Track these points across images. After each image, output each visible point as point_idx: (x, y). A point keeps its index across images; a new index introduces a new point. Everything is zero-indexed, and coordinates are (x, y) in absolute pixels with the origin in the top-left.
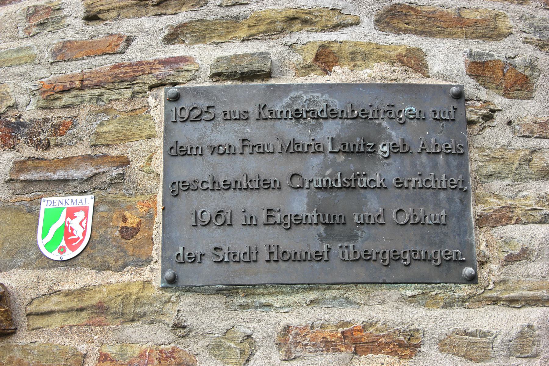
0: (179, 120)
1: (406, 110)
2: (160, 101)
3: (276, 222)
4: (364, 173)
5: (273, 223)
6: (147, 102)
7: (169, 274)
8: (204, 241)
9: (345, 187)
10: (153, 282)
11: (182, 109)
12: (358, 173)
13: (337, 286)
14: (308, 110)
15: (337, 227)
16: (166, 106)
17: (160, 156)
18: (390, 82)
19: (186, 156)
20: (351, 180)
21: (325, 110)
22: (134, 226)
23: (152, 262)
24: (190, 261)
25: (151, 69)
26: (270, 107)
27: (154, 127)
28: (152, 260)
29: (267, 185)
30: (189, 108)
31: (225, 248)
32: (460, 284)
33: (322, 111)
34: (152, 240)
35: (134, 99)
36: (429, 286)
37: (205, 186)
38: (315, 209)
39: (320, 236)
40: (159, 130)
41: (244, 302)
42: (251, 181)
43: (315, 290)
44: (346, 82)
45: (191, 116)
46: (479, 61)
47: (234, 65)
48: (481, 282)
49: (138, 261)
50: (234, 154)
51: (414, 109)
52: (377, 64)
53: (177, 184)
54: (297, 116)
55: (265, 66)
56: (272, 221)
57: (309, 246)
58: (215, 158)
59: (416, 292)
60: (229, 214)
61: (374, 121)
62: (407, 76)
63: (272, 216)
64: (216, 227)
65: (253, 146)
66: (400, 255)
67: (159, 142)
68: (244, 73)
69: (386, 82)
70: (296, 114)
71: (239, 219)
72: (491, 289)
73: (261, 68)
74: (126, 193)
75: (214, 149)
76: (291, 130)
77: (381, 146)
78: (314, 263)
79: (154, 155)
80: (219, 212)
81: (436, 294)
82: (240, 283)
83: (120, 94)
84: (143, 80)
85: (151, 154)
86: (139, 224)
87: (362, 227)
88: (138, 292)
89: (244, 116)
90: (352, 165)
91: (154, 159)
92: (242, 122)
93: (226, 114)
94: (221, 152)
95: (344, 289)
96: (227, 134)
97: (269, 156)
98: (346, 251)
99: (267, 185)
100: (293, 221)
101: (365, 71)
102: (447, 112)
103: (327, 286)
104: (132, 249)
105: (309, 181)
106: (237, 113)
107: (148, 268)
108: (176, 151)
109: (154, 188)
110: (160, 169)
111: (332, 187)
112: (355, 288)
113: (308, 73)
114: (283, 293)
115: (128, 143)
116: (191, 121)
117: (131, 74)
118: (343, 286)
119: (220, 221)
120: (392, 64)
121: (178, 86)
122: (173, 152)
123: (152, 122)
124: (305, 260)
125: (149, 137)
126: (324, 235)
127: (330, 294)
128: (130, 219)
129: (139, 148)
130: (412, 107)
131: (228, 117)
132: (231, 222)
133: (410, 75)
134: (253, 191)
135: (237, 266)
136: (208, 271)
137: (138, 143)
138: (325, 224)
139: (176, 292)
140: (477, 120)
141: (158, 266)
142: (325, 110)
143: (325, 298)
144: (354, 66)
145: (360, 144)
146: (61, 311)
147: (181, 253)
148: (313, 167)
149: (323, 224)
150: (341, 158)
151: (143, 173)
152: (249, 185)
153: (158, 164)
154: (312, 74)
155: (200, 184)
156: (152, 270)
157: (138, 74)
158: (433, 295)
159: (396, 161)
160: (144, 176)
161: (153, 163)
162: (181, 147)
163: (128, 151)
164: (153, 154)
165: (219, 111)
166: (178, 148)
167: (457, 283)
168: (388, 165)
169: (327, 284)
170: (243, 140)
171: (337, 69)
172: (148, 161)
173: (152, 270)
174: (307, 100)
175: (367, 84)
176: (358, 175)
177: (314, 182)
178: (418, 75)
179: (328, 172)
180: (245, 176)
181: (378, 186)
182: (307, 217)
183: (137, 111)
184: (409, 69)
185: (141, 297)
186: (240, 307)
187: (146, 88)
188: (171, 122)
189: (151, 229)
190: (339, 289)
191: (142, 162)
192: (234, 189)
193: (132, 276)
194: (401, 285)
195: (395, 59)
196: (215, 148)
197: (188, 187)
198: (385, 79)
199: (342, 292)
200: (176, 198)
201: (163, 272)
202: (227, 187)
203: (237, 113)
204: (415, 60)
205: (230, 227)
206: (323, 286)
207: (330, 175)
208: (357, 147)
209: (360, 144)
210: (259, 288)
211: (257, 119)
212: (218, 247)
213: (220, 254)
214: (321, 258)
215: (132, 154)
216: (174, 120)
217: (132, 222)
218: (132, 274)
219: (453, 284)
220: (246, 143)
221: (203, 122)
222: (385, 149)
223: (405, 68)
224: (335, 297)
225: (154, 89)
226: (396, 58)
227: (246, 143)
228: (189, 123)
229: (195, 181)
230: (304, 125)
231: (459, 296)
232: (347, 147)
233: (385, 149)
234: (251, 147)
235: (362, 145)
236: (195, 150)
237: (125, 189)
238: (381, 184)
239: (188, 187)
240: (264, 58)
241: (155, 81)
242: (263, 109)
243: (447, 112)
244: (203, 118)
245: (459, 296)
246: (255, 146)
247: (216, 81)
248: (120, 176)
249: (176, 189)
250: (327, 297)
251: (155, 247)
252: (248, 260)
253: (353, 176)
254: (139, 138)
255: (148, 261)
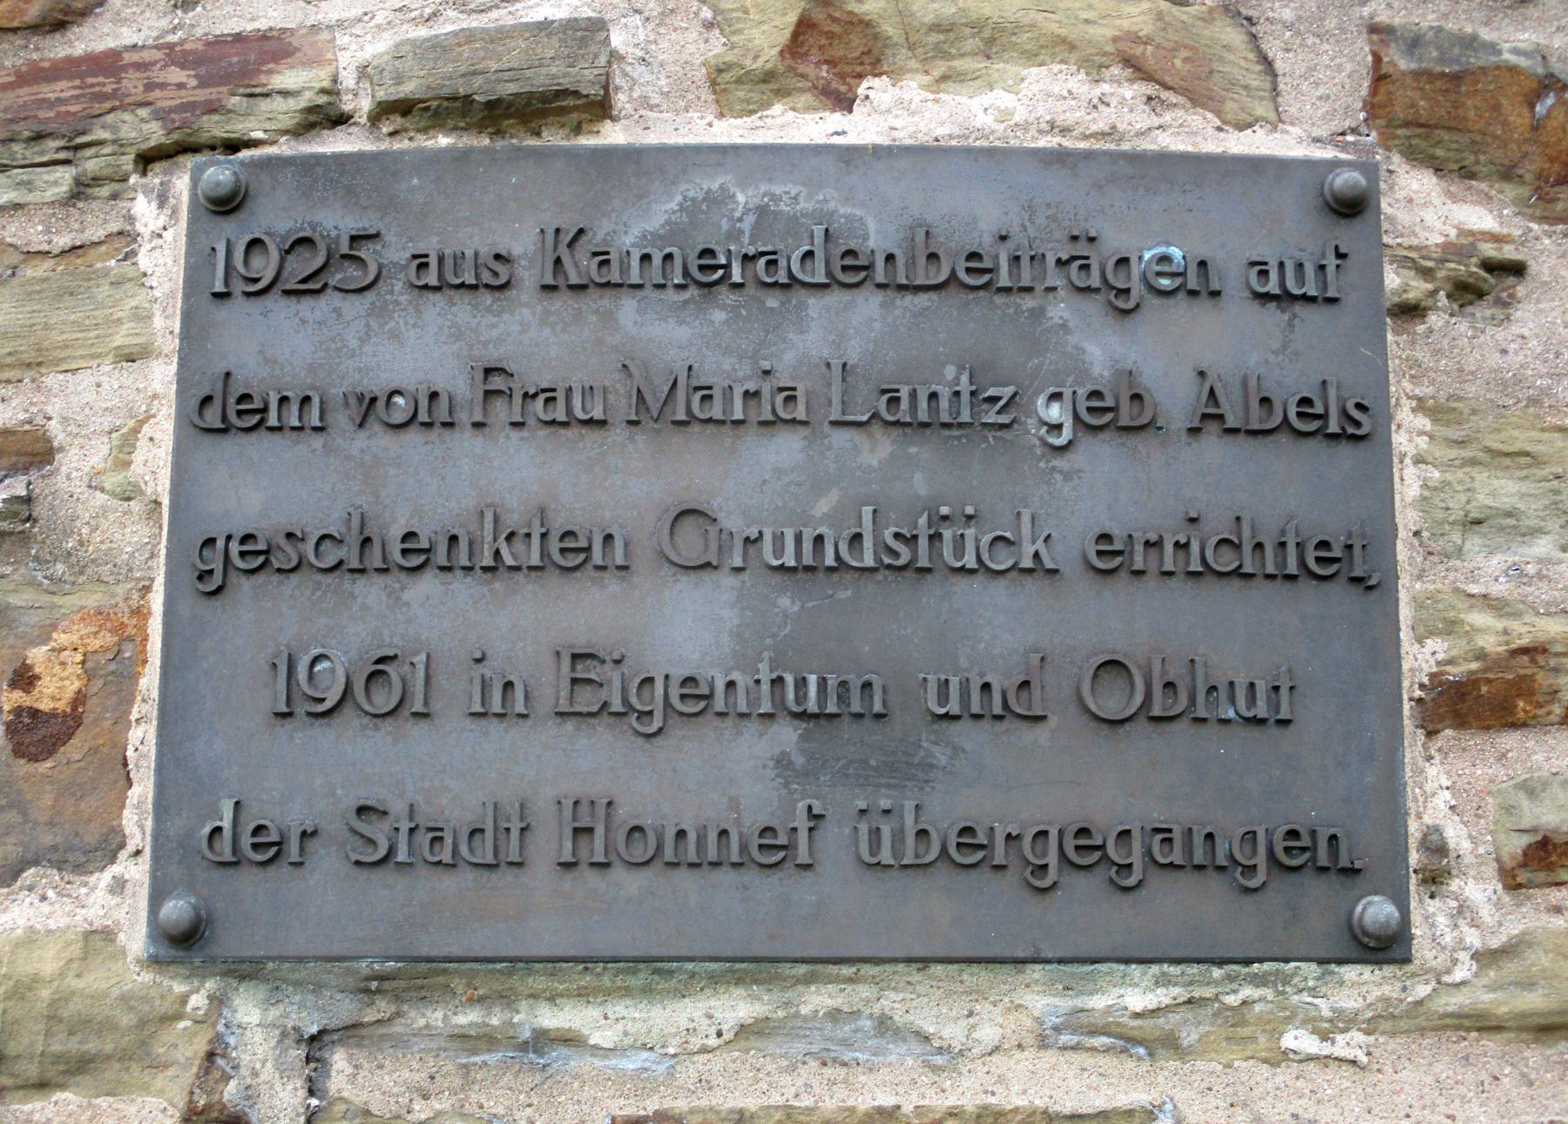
0: (239, 287)
1: (1147, 256)
2: (175, 212)
3: (605, 705)
4: (970, 510)
5: (595, 709)
6: (131, 219)
7: (176, 909)
8: (315, 775)
9: (889, 567)
10: (122, 936)
11: (255, 243)
12: (944, 510)
13: (847, 971)
14: (751, 251)
15: (848, 729)
16: (191, 235)
17: (163, 428)
18: (1083, 145)
19: (262, 432)
20: (915, 537)
21: (820, 255)
22: (62, 706)
23: (123, 855)
24: (259, 858)
25: (150, 87)
26: (599, 238)
27: (150, 317)
28: (122, 846)
29: (574, 554)
30: (283, 242)
31: (397, 807)
32: (1341, 962)
33: (809, 255)
34: (126, 765)
35: (80, 205)
36: (1217, 973)
37: (331, 556)
38: (766, 655)
39: (782, 762)
40: (166, 327)
41: (471, 1024)
42: (510, 537)
43: (756, 982)
44: (908, 142)
45: (285, 274)
46: (1438, 69)
47: (463, 69)
48: (1423, 950)
49: (70, 849)
50: (449, 425)
51: (1176, 253)
52: (1034, 70)
53: (220, 543)
54: (707, 274)
55: (584, 77)
56: (587, 700)
57: (734, 804)
58: (377, 441)
59: (1162, 997)
60: (421, 673)
61: (1015, 299)
62: (1156, 121)
63: (590, 681)
64: (366, 720)
65: (526, 395)
66: (1102, 847)
67: (162, 375)
68: (499, 101)
69: (1068, 143)
70: (702, 268)
71: (456, 691)
72: (1463, 983)
73: (566, 83)
74: (39, 576)
75: (368, 407)
76: (672, 335)
77: (1041, 401)
78: (751, 876)
79: (146, 428)
80: (381, 660)
81: (1244, 1003)
82: (456, 951)
83: (28, 185)
84: (114, 128)
85: (131, 423)
86: (79, 699)
87: (955, 727)
88: (62, 974)
89: (496, 274)
90: (920, 475)
91: (142, 443)
92: (487, 298)
93: (423, 266)
94: (398, 417)
95: (874, 980)
96: (420, 347)
97: (592, 436)
98: (886, 830)
99: (574, 554)
100: (675, 701)
101: (989, 98)
102: (1310, 270)
103: (802, 969)
104: (48, 801)
105: (747, 540)
106: (469, 263)
107: (105, 878)
108: (225, 412)
109: (140, 558)
110: (161, 486)
111: (841, 565)
112: (917, 977)
113: (766, 105)
114: (627, 992)
115: (52, 380)
116: (288, 293)
117: (73, 109)
118: (869, 970)
119: (383, 700)
120: (1094, 67)
121: (245, 154)
122: (213, 417)
123: (140, 299)
124: (715, 865)
125: (130, 357)
126: (799, 760)
127: (818, 999)
128: (46, 680)
129: (90, 397)
130: (1169, 244)
131: (439, 278)
132: (426, 703)
133: (1168, 117)
134: (519, 577)
135: (448, 883)
136: (326, 901)
137: (86, 378)
138: (803, 716)
139: (204, 978)
140: (1430, 302)
141: (136, 871)
142: (820, 255)
143: (797, 1015)
144: (945, 78)
145: (957, 394)
146: (317, 959)
147: (226, 824)
148: (755, 480)
149: (795, 715)
150: (877, 451)
151: (101, 498)
152: (505, 552)
153: (155, 461)
154: (777, 108)
155: (309, 548)
156: (119, 886)
157: (98, 108)
158: (1233, 1008)
159: (1101, 460)
160: (104, 509)
161: (138, 457)
162: (245, 397)
163: (49, 409)
164: (142, 423)
165: (395, 250)
166: (232, 400)
167: (1328, 962)
168: (1067, 476)
169: (804, 961)
170: (488, 371)
171: (876, 89)
172: (121, 448)
173: (119, 886)
174: (747, 211)
175: (991, 152)
176: (945, 518)
177: (767, 545)
178: (1201, 120)
179: (823, 507)
180: (489, 517)
181: (1027, 563)
182: (731, 685)
183: (93, 253)
184: (1164, 95)
185: (73, 993)
186: (456, 1045)
187: (127, 162)
188: (215, 291)
189: (122, 722)
190: (851, 980)
191: (99, 454)
192: (442, 569)
193: (45, 908)
194: (1104, 967)
195: (1105, 54)
196: (374, 400)
197: (261, 559)
198: (1065, 131)
199: (864, 991)
200: (216, 603)
201: (157, 897)
202: (417, 556)
203: (469, 263)
204: (1185, 60)
205: (424, 725)
206: (786, 969)
207: (828, 518)
208: (944, 404)
209: (957, 394)
210: (530, 972)
211: (547, 288)
212: (369, 803)
213: (379, 831)
214: (781, 854)
215: (65, 420)
216: (219, 287)
217: (53, 692)
218: (44, 898)
219: (1313, 966)
220: (497, 382)
221: (330, 300)
222: (1055, 412)
223: (1150, 89)
224: (835, 1015)
225: (158, 167)
226: (1110, 48)
227: (497, 382)
228: (274, 302)
229: (290, 535)
230: (735, 309)
231: (1333, 1010)
232: (904, 405)
233: (1055, 412)
234: (517, 399)
235: (965, 397)
236: (295, 408)
237: (37, 559)
238: (1036, 555)
239: (261, 559)
240: (583, 43)
241: (156, 134)
242: (570, 245)
243: (1310, 270)
244: (332, 282)
245: (1333, 1010)
246: (535, 395)
247: (391, 134)
248: (16, 507)
249: (218, 566)
250: (804, 1010)
251: (135, 793)
252: (490, 859)
253: (923, 521)
254: (93, 357)
255: (110, 847)
